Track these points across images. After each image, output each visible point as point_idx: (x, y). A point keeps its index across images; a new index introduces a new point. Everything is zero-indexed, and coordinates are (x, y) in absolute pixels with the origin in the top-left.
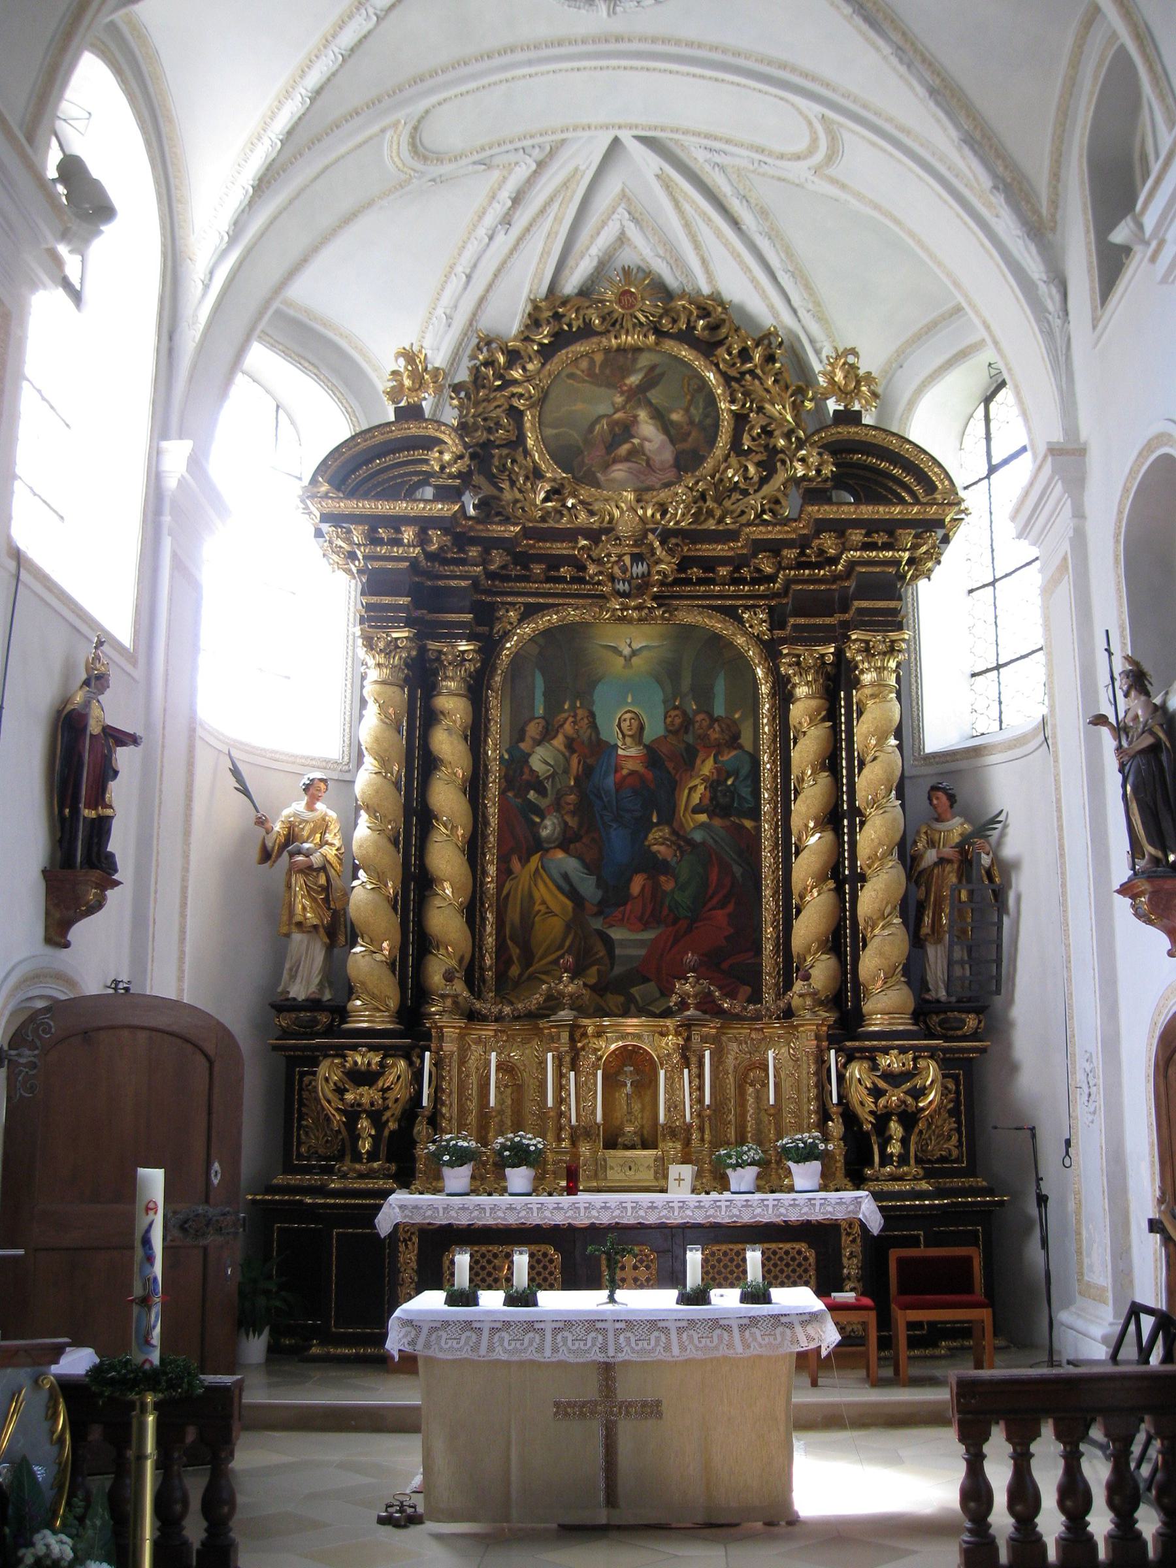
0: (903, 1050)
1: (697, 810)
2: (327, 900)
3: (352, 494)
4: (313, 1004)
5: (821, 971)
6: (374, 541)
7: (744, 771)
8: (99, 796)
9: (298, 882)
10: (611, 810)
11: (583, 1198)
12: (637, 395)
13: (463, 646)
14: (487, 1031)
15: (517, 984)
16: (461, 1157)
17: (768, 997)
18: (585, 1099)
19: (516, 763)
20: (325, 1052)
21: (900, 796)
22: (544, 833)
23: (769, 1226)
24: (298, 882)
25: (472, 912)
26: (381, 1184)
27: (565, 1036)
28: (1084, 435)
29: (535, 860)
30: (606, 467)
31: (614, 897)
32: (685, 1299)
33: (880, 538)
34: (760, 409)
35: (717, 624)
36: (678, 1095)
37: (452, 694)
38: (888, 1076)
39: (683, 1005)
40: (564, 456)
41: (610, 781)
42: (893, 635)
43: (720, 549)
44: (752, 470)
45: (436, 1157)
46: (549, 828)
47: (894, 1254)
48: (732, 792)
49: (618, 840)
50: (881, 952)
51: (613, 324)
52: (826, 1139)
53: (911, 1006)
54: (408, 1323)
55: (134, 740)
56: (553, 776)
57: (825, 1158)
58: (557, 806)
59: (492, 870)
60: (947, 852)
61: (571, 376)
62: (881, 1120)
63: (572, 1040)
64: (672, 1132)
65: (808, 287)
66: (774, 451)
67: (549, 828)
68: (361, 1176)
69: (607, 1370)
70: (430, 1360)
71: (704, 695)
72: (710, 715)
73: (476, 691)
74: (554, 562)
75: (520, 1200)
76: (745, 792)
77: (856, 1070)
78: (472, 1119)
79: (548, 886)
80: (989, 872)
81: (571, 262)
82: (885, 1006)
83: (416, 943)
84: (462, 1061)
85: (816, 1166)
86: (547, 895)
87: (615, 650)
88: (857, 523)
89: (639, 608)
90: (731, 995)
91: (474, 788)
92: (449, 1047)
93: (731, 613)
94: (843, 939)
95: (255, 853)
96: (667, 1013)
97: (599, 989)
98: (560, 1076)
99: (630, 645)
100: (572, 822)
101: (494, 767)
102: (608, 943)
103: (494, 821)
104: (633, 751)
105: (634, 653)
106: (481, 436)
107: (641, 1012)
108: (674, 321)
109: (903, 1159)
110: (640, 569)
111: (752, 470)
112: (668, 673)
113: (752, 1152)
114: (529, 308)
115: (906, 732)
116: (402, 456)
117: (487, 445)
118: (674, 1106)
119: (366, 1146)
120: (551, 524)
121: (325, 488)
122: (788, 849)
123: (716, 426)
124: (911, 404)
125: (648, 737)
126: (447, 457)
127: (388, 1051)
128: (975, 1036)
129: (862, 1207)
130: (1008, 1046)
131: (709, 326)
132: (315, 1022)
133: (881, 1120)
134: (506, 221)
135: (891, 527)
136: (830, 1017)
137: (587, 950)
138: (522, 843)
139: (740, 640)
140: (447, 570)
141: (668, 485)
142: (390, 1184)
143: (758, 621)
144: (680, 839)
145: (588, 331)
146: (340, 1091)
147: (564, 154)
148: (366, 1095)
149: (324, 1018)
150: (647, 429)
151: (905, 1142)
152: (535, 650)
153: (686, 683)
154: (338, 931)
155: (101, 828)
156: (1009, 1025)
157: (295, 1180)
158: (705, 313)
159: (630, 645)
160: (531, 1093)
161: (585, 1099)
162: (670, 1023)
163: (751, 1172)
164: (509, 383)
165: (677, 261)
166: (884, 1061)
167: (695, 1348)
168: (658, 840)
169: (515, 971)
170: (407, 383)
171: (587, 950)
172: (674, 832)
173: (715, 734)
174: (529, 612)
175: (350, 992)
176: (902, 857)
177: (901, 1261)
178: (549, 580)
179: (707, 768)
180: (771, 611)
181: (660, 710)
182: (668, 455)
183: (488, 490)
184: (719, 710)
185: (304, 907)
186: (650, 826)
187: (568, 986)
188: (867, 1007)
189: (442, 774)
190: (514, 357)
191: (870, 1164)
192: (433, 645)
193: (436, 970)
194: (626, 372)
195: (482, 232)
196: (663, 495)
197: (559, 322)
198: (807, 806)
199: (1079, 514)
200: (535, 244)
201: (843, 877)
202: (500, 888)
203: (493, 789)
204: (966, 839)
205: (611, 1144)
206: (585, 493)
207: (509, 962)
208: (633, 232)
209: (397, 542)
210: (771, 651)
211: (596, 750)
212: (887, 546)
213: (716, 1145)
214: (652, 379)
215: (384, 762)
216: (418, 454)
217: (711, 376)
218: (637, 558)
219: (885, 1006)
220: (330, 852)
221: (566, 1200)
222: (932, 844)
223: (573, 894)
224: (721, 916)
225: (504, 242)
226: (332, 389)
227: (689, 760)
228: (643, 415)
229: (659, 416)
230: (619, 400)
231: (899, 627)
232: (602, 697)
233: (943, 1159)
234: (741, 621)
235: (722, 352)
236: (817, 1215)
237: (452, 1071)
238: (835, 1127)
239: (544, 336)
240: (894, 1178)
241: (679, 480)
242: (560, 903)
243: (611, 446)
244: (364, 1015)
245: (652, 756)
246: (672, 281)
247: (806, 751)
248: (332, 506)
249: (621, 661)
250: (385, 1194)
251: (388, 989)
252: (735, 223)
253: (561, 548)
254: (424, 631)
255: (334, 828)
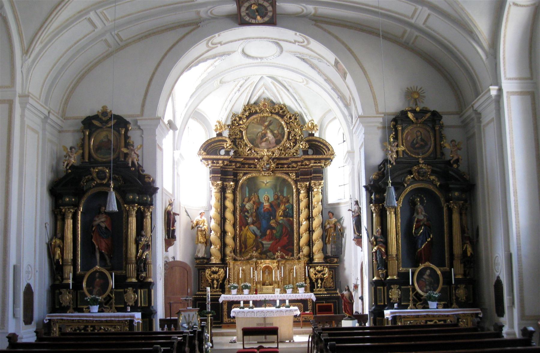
0: (321, 266)
1: (281, 216)
2: (205, 237)
3: (208, 154)
4: (203, 258)
5: (305, 250)
6: (213, 163)
7: (291, 207)
8: (173, 226)
9: (199, 233)
10: (263, 217)
11: (258, 295)
12: (267, 127)
13: (232, 183)
14: (239, 263)
15: (244, 253)
16: (235, 288)
17: (295, 255)
18: (258, 276)
19: (243, 207)
20: (207, 268)
21: (322, 214)
22: (249, 221)
23: (294, 300)
24: (199, 233)
25: (234, 239)
26: (219, 293)
27: (254, 264)
28: (355, 149)
29: (247, 227)
30: (261, 143)
31: (264, 234)
32: (277, 307)
33: (317, 162)
34: (294, 130)
35: (285, 176)
36: (277, 275)
37: (229, 193)
38: (318, 271)
39: (278, 257)
40: (252, 141)
41: (262, 210)
42: (320, 181)
43: (285, 162)
44: (292, 144)
45: (230, 288)
46: (250, 220)
47: (317, 305)
48: (288, 212)
49: (264, 222)
50: (317, 246)
51: (262, 111)
52: (306, 283)
53: (323, 257)
54: (234, 312)
55: (178, 215)
56: (250, 209)
57: (305, 287)
58: (251, 216)
59: (238, 229)
60: (331, 225)
61: (253, 123)
62: (317, 280)
63: (256, 264)
64: (276, 282)
65: (304, 102)
66: (296, 140)
67: (250, 220)
68: (215, 292)
69: (265, 318)
70: (238, 317)
71: (282, 192)
72: (283, 196)
73: (234, 192)
74: (250, 164)
75: (246, 295)
76: (291, 212)
77: (312, 270)
78: (236, 280)
79: (250, 232)
80: (340, 230)
81: (252, 97)
82: (318, 257)
83: (224, 245)
84: (234, 269)
85: (303, 288)
86: (250, 235)
87: (263, 182)
88: (313, 159)
89: (268, 173)
90: (287, 255)
91: (234, 213)
92: (231, 266)
93: (287, 174)
94: (310, 243)
95: (191, 227)
96: (274, 259)
97: (261, 254)
98: (253, 271)
99: (266, 181)
100: (255, 219)
101: (238, 208)
102: (263, 244)
103: (238, 219)
104: (267, 204)
105: (267, 183)
106: (234, 137)
107: (270, 258)
108: (275, 110)
109: (321, 287)
110: (268, 166)
111: (292, 144)
112: (275, 187)
113: (291, 286)
114: (243, 107)
115: (323, 201)
116: (218, 143)
117: (235, 139)
118: (276, 277)
119: (215, 286)
120: (249, 157)
121: (202, 152)
122: (299, 224)
123: (284, 134)
124: (327, 126)
125: (271, 200)
126: (228, 145)
127: (219, 267)
128: (336, 263)
129: (312, 296)
130: (344, 264)
131: (281, 111)
132: (203, 261)
133: (317, 280)
134: (239, 90)
135: (320, 160)
136: (307, 259)
137: (258, 246)
138: (244, 223)
139: (290, 180)
140: (228, 167)
141: (274, 147)
142: (220, 293)
143: (293, 176)
144: (277, 222)
145: (256, 112)
146: (210, 275)
147: (250, 79)
148: (216, 276)
149: (206, 261)
150: (269, 135)
151: (321, 284)
152: (246, 182)
153: (278, 189)
154: (208, 243)
155: (174, 231)
156: (344, 260)
157: (200, 293)
158: (282, 109)
159: (266, 181)
160: (248, 275)
161: (258, 276)
162: (275, 261)
163: (291, 290)
164: (240, 124)
165: (275, 96)
166: (317, 268)
167: (278, 315)
168: (272, 223)
169: (243, 250)
170: (219, 128)
171: (258, 246)
172: (276, 221)
173: (284, 200)
174: (245, 174)
175: (211, 255)
176: (322, 227)
177: (319, 306)
178: (249, 167)
179: (283, 207)
180: (296, 173)
181: (273, 195)
182: (274, 141)
183: (236, 149)
184: (285, 195)
185: (201, 239)
186: (271, 220)
187: (255, 254)
188: (314, 257)
189: (228, 210)
190: (240, 119)
191: (315, 288)
192: (225, 183)
193: (228, 251)
194: (264, 122)
195: (233, 92)
196: (273, 149)
197: (251, 110)
198: (303, 216)
199: (353, 164)
200: (245, 95)
201: (310, 231)
202: (240, 233)
203: (238, 212)
204: (336, 222)
205: (264, 285)
206: (256, 149)
207: (242, 248)
208: (266, 91)
209: (218, 163)
210: (296, 182)
211: (259, 204)
212: (319, 163)
213: (284, 285)
214: (270, 123)
215: (216, 209)
216: (221, 143)
217: (283, 123)
218: (267, 164)
219: (318, 257)
220: (205, 227)
221: (255, 295)
222: (329, 223)
223: (255, 234)
224: (286, 238)
225: (238, 94)
226: (201, 123)
227: (279, 205)
228: (268, 131)
229: (272, 131)
230: (263, 128)
231: (322, 179)
232: (260, 192)
233: (330, 287)
234: (289, 175)
235: (285, 117)
236: (303, 298)
237: (232, 271)
238: (308, 281)
239: (247, 114)
240: (319, 291)
241: (276, 146)
242: (253, 236)
243: (262, 139)
244: (214, 260)
245: (271, 205)
246: (274, 101)
247: (303, 204)
248: (205, 157)
249: (264, 185)
250: (220, 295)
251: (219, 254)
252: (288, 90)
253: (251, 162)
254: (223, 180)
255: (206, 222)
